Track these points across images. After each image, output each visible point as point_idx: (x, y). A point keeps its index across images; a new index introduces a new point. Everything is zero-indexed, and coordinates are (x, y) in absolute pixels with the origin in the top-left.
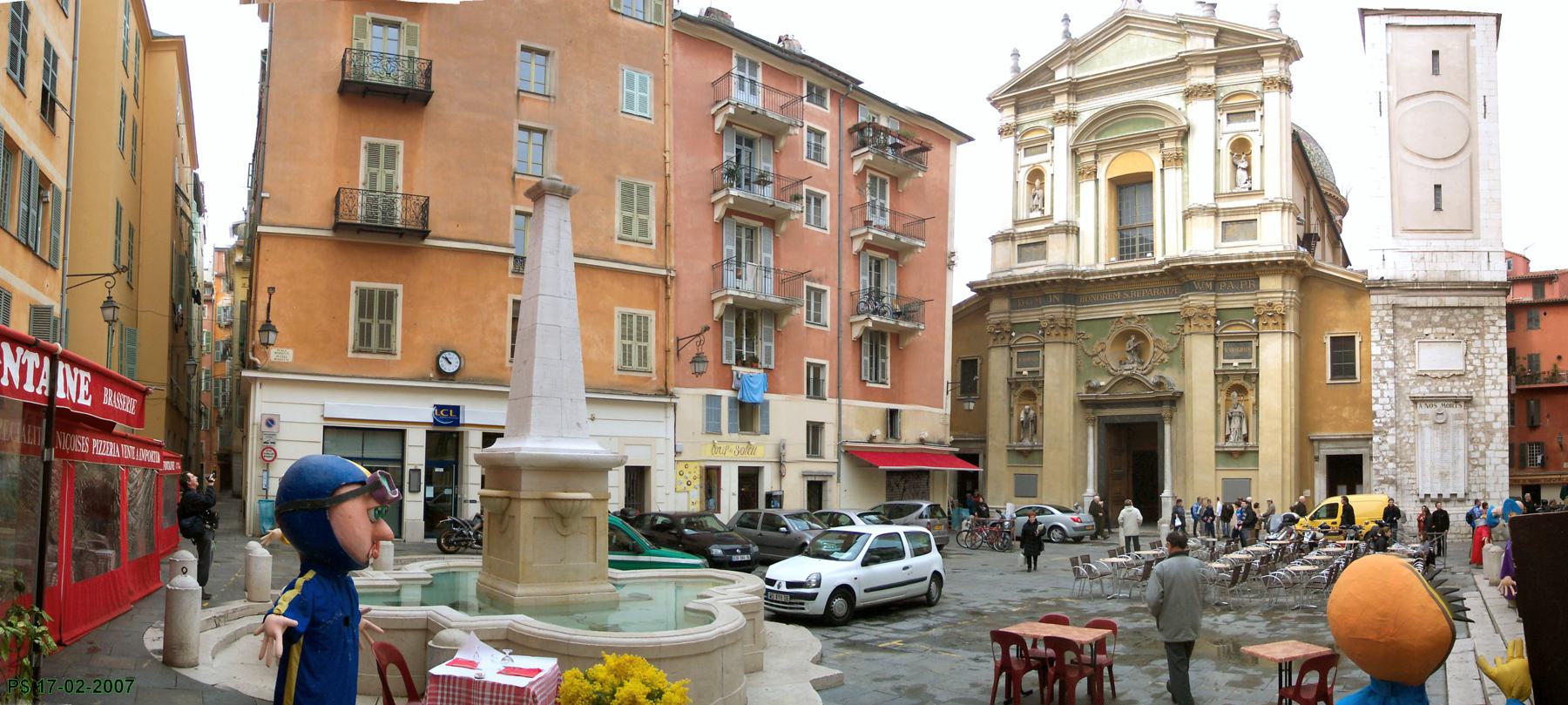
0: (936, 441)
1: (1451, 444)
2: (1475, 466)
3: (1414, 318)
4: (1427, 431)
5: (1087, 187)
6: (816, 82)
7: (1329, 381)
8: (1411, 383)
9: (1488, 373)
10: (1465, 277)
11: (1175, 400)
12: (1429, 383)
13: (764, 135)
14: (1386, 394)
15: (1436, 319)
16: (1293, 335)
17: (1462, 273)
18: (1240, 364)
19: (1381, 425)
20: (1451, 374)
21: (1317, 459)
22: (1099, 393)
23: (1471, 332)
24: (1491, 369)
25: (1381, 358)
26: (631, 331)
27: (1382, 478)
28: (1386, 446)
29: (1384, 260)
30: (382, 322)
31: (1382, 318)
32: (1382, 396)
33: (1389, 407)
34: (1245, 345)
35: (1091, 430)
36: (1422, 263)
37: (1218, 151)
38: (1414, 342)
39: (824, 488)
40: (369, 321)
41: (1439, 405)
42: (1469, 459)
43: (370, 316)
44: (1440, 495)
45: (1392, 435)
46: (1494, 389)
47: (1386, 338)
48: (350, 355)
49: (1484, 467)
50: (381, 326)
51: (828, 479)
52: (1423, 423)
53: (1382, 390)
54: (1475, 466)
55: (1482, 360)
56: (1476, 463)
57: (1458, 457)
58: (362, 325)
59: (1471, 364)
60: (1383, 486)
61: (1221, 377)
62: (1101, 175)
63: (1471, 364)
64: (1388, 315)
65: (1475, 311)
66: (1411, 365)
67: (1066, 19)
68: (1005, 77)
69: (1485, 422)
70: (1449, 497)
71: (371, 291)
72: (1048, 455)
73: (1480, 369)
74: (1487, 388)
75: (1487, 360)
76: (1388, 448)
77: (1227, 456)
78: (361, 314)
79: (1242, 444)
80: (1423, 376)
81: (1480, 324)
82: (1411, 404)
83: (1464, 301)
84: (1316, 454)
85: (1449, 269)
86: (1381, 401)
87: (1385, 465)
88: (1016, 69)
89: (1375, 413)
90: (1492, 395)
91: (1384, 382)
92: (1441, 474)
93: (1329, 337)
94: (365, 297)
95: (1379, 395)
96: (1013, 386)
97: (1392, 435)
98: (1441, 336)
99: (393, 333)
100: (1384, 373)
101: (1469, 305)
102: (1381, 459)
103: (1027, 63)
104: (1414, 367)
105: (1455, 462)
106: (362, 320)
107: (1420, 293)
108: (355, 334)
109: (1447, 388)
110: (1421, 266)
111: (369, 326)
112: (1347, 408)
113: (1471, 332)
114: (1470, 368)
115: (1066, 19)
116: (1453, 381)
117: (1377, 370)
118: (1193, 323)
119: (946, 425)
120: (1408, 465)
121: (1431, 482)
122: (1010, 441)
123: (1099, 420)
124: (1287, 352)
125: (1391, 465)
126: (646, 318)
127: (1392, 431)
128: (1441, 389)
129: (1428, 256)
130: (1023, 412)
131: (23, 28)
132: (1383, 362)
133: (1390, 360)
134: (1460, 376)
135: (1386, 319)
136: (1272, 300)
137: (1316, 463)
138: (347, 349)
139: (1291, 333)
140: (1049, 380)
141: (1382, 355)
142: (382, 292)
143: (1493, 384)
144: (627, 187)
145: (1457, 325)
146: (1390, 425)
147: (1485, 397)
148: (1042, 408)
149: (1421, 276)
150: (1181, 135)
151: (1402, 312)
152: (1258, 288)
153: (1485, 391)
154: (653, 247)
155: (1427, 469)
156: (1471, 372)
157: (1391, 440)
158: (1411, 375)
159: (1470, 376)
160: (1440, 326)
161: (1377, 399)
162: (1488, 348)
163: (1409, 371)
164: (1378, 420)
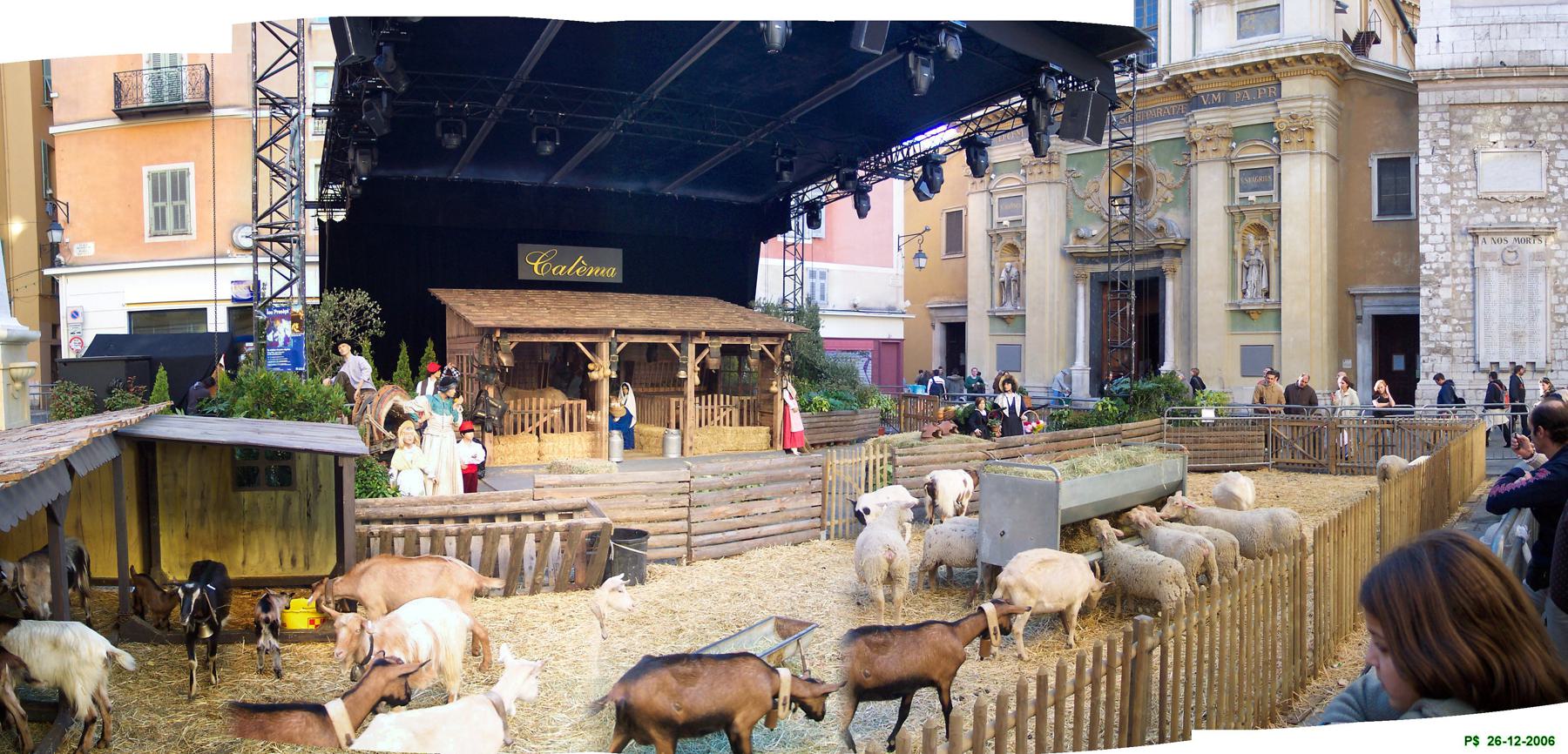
0: (883, 306)
1: (1527, 296)
4: (1495, 277)
7: (1375, 218)
8: (1469, 211)
10: (1546, 59)
11: (1182, 249)
12: (1498, 209)
14: (1439, 230)
15: (1506, 120)
16: (1325, 157)
19: (1432, 273)
20: (1527, 197)
21: (1359, 319)
22: (1090, 244)
25: (1433, 180)
27: (1432, 346)
28: (1436, 302)
29: (1438, 41)
30: (175, 203)
31: (1434, 124)
32: (1433, 232)
33: (1443, 248)
34: (1265, 177)
35: (1081, 290)
36: (1487, 41)
40: (163, 204)
41: (1511, 239)
42: (1554, 314)
43: (164, 198)
45: (1448, 286)
47: (1440, 152)
48: (148, 240)
50: (175, 208)
52: (1488, 264)
53: (1434, 225)
56: (1562, 320)
57: (1537, 312)
58: (156, 209)
59: (1555, 183)
60: (1434, 356)
61: (1235, 215)
63: (1555, 183)
64: (1443, 119)
71: (163, 175)
72: (1030, 322)
76: (1441, 304)
77: (1242, 315)
78: (155, 199)
79: (1262, 300)
80: (1489, 201)
83: (1545, 95)
84: (1359, 313)
85: (1524, 49)
86: (1431, 239)
87: (1436, 328)
89: (1423, 256)
91: (1437, 214)
92: (1515, 334)
93: (1376, 159)
94: (157, 180)
96: (994, 239)
97: (1448, 286)
98: (1514, 144)
99: (187, 213)
100: (1436, 200)
101: (1551, 100)
102: (1431, 318)
105: (1533, 319)
106: (156, 204)
107: (1484, 83)
108: (151, 218)
109: (1522, 218)
110: (1485, 46)
111: (163, 209)
112: (1399, 253)
114: (1554, 189)
116: (1531, 207)
117: (1427, 196)
118: (1200, 148)
119: (898, 287)
121: (1501, 347)
122: (992, 306)
123: (1092, 277)
124: (1317, 179)
125: (1445, 328)
127: (1446, 281)
128: (1513, 218)
129: (1494, 31)
130: (1004, 271)
132: (1435, 185)
133: (1445, 182)
134: (1541, 200)
135: (1440, 125)
136: (1296, 110)
137: (1359, 325)
138: (143, 235)
140: (1032, 231)
141: (1433, 176)
142: (173, 174)
145: (1536, 129)
146: (1444, 272)
148: (1024, 265)
149: (1485, 59)
151: (1460, 113)
152: (1280, 96)
155: (1495, 327)
157: (1445, 293)
158: (1470, 199)
159: (1554, 200)
160: (1513, 130)
161: (1426, 237)
163: (1467, 193)
164: (1428, 266)
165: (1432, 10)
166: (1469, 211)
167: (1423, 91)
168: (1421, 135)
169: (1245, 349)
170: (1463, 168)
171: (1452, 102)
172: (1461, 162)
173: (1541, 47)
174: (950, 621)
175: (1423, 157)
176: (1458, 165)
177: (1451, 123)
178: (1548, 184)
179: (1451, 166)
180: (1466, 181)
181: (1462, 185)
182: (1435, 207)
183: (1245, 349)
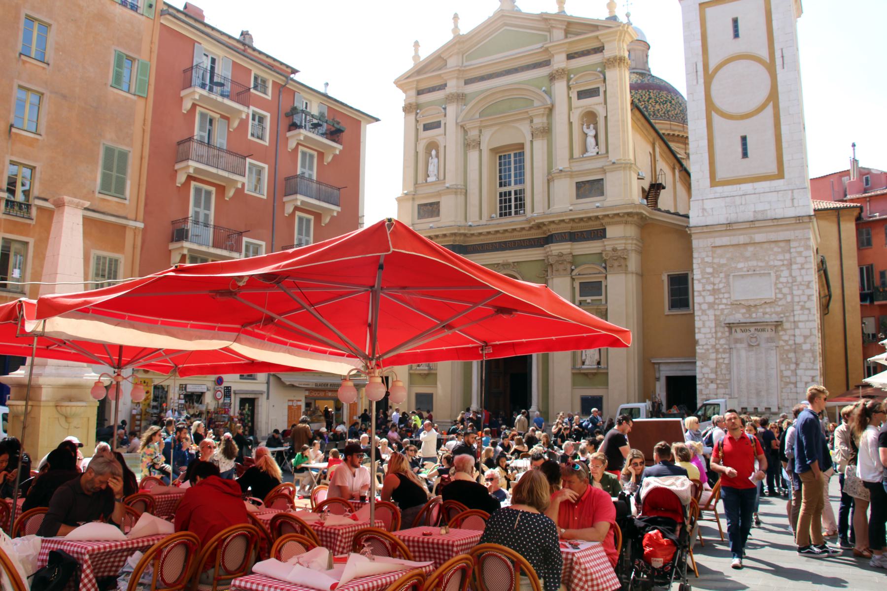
2: (787, 383)
3: (729, 255)
5: (473, 155)
6: (262, 74)
9: (796, 299)
13: (223, 117)
14: (707, 324)
17: (769, 211)
18: (592, 300)
21: (658, 379)
23: (780, 263)
25: (703, 293)
26: (104, 270)
32: (704, 326)
37: (571, 124)
38: (729, 275)
39: (256, 404)
44: (756, 409)
46: (803, 314)
49: (795, 384)
51: (260, 396)
52: (738, 346)
54: (787, 383)
55: (791, 289)
62: (485, 147)
65: (782, 244)
66: (726, 295)
67: (456, 17)
68: (408, 65)
69: (795, 344)
70: (764, 410)
73: (789, 298)
74: (796, 313)
75: (795, 288)
80: (736, 305)
81: (787, 256)
82: (727, 329)
84: (657, 375)
86: (703, 330)
88: (416, 57)
90: (801, 320)
95: (701, 289)
100: (705, 306)
102: (704, 380)
103: (425, 53)
104: (730, 298)
113: (780, 263)
114: (779, 296)
115: (456, 17)
117: (700, 304)
120: (723, 382)
126: (116, 261)
131: (467, 308)
132: (704, 297)
133: (710, 295)
139: (632, 273)
141: (704, 291)
143: (801, 310)
144: (109, 152)
147: (794, 322)
150: (547, 112)
153: (794, 316)
154: (127, 202)
156: (780, 299)
158: (726, 304)
159: (780, 303)
162: (795, 277)
164: (701, 347)
166: (726, 312)
170: (721, 285)
172: (720, 282)
175: (697, 280)
178: (776, 293)
179: (714, 284)
181: (721, 296)
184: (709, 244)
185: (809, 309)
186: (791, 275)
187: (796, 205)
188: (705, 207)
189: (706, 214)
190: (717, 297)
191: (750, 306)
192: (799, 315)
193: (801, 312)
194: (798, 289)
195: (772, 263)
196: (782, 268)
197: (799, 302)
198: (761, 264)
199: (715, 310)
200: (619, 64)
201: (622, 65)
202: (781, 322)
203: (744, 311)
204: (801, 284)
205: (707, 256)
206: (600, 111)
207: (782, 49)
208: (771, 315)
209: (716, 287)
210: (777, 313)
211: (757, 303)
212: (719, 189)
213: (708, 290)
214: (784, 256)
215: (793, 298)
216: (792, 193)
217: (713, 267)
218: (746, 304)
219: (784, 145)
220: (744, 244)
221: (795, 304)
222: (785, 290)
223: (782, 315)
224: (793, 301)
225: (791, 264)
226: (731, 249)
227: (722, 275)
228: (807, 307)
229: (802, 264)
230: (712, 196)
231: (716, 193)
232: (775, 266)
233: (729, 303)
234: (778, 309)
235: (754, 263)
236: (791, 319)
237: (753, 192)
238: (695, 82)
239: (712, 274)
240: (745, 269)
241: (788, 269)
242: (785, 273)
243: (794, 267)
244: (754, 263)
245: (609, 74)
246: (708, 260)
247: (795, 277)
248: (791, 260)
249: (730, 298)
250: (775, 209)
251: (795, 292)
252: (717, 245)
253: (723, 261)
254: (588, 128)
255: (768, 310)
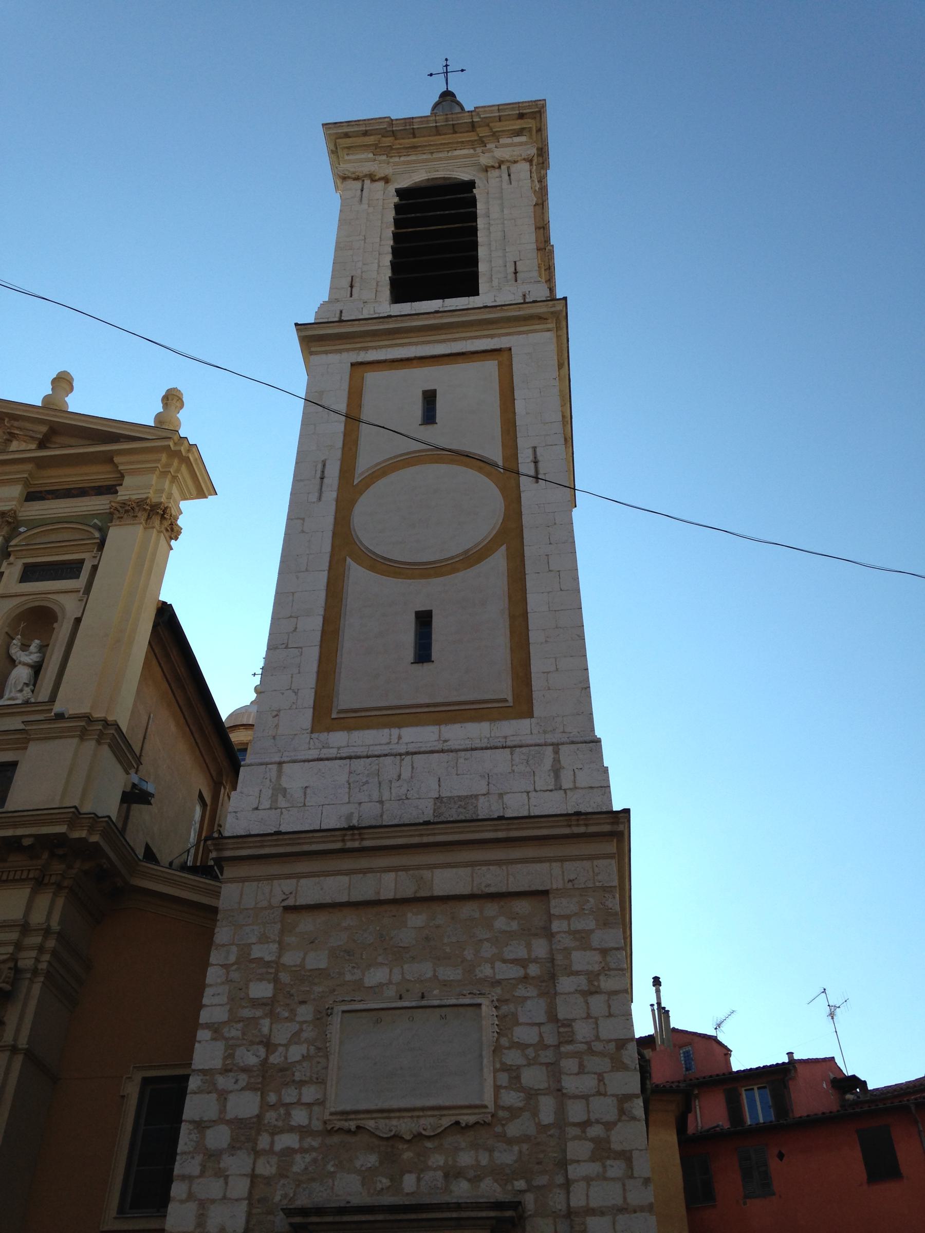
8: (299, 1163)
9: (576, 1112)
10: (487, 808)
17: (482, 799)
23: (515, 972)
24: (585, 1097)
25: (222, 1082)
38: (329, 1013)
65: (522, 907)
66: (310, 1094)
73: (547, 1109)
74: (574, 1171)
75: (570, 1065)
81: (540, 948)
100: (219, 1137)
113: (515, 972)
114: (511, 1098)
117: (201, 1126)
132: (223, 1096)
133: (249, 1087)
141: (226, 1070)
153: (567, 1185)
156: (514, 1113)
158: (304, 1131)
159: (513, 1130)
165: (274, 738)
166: (299, 1163)
167: (233, 880)
168: (213, 974)
169: (476, 293)
170: (296, 1053)
171: (290, 902)
172: (295, 1038)
173: (481, 787)
174: (221, 964)
175: (207, 1026)
176: (287, 1046)
177: (282, 947)
178: (497, 1088)
179: (269, 1045)
180: (302, 1083)
181: (290, 1095)
182: (213, 1156)
183: (476, 293)
184: (276, 901)
185: (626, 1157)
186: (552, 1017)
187: (567, 783)
188: (285, 782)
189: (282, 803)
190: (272, 1098)
191: (397, 1137)
192: (588, 1180)
193: (593, 1168)
194: (582, 1071)
195: (486, 971)
196: (521, 991)
197: (585, 1124)
198: (450, 973)
199: (257, 1154)
200: (149, 517)
201: (156, 521)
202: (516, 1205)
203: (372, 1160)
204: (591, 1051)
205: (264, 939)
206: (69, 606)
207: (534, 449)
208: (475, 1180)
209: (275, 1059)
210: (500, 1174)
211: (427, 1124)
212: (338, 739)
213: (245, 1070)
214: (529, 946)
215: (561, 1110)
216: (556, 752)
217: (276, 980)
218: (383, 1127)
219: (535, 636)
220: (394, 902)
221: (572, 1131)
222: (534, 1077)
223: (521, 1184)
224: (561, 1122)
225: (553, 977)
226: (350, 919)
227: (305, 1012)
228: (616, 1146)
229: (593, 976)
230: (314, 754)
231: (326, 746)
232: (498, 982)
233: (317, 1125)
234: (506, 1157)
235: (425, 969)
236: (557, 1201)
237: (439, 746)
238: (314, 497)
239: (269, 1006)
240: (391, 992)
241: (541, 995)
242: (535, 1009)
243: (566, 984)
244: (425, 969)
245: (114, 533)
246: (265, 952)
247: (568, 1023)
248: (552, 960)
249: (321, 1103)
250: (501, 795)
251: (571, 1084)
252: (301, 901)
253: (317, 960)
254: (25, 647)
255: (466, 1159)
